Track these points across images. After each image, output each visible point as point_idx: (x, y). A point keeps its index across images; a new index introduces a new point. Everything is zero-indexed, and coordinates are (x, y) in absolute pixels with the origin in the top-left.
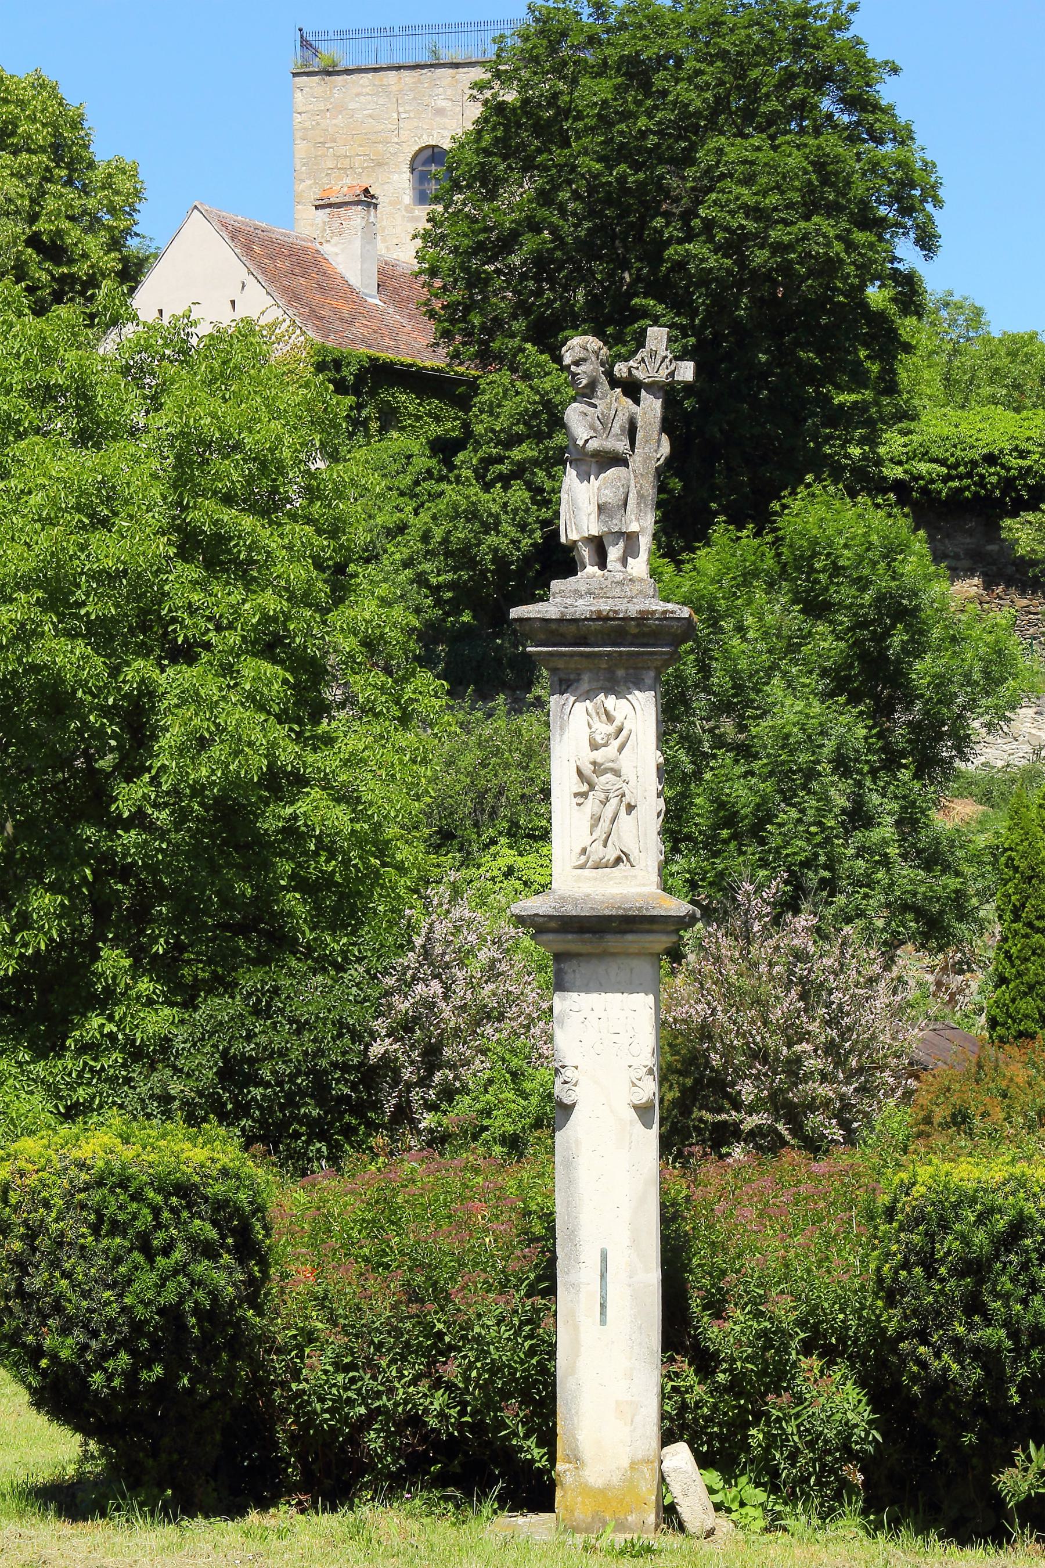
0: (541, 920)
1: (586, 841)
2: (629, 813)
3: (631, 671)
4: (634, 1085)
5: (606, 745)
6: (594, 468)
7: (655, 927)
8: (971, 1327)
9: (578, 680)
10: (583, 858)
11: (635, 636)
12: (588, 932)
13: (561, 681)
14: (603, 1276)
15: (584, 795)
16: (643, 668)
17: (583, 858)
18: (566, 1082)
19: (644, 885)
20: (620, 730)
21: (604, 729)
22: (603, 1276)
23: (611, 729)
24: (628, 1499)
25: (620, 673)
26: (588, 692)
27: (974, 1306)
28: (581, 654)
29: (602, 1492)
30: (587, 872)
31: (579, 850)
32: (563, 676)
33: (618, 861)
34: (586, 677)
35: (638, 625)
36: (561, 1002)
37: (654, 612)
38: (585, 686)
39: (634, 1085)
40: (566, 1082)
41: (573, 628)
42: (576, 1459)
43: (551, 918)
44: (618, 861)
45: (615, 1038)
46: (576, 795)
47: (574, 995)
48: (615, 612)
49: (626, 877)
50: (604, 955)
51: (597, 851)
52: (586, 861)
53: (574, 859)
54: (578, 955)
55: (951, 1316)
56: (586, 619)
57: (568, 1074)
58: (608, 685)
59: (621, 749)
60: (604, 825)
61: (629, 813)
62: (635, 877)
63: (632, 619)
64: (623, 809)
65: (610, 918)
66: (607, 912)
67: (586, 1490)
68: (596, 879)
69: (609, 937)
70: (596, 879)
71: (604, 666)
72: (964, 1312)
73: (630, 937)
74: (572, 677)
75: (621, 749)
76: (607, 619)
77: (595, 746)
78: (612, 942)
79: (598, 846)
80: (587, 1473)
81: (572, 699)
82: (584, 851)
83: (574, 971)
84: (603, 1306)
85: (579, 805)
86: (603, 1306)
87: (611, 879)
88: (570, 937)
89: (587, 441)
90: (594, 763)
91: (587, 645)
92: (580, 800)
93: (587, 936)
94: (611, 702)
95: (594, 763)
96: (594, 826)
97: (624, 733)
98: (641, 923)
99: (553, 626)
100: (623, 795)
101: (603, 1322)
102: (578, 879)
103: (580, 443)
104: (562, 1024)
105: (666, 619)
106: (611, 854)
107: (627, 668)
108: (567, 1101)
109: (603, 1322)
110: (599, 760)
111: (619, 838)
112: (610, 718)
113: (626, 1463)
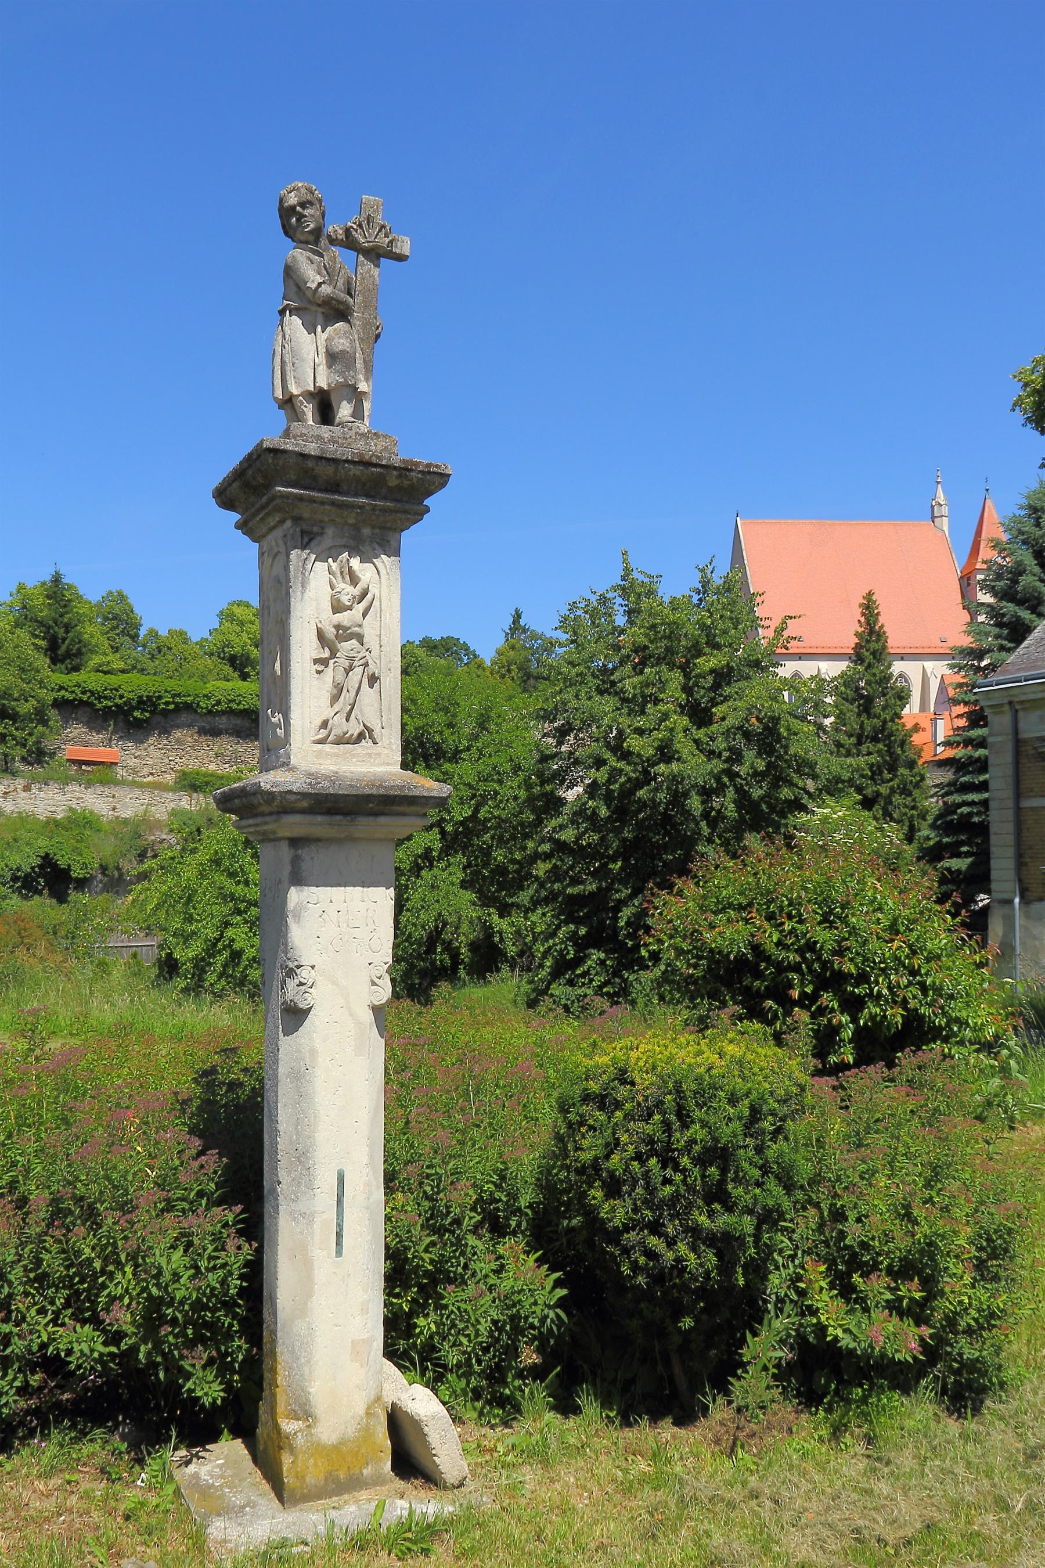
0: (292, 798)
1: (328, 713)
2: (371, 686)
3: (377, 531)
4: (374, 984)
5: (350, 608)
6: (320, 318)
7: (413, 809)
8: (711, 1214)
9: (322, 534)
10: (323, 733)
11: (391, 490)
12: (336, 813)
13: (303, 532)
14: (340, 1202)
15: (324, 662)
16: (390, 529)
17: (323, 733)
18: (301, 984)
19: (388, 764)
20: (364, 593)
21: (347, 592)
22: (340, 1202)
23: (357, 591)
24: (363, 1451)
25: (366, 531)
26: (330, 548)
27: (717, 1196)
28: (333, 503)
29: (336, 1447)
30: (327, 748)
31: (318, 722)
32: (305, 527)
33: (361, 737)
34: (330, 531)
35: (400, 476)
36: (295, 896)
37: (418, 464)
38: (329, 538)
39: (374, 984)
40: (301, 984)
41: (330, 470)
42: (305, 1413)
43: (304, 795)
44: (361, 737)
45: (356, 932)
46: (316, 661)
47: (313, 889)
48: (378, 457)
49: (370, 755)
50: (352, 839)
51: (339, 725)
52: (327, 735)
53: (313, 733)
54: (318, 840)
55: (690, 1205)
56: (347, 461)
57: (304, 974)
58: (352, 543)
59: (364, 615)
60: (346, 697)
61: (371, 686)
62: (379, 754)
63: (395, 468)
64: (365, 680)
65: (368, 798)
66: (367, 791)
67: (319, 1449)
68: (337, 755)
69: (362, 821)
70: (337, 755)
71: (351, 521)
72: (704, 1199)
73: (383, 820)
74: (315, 529)
75: (364, 615)
76: (368, 464)
77: (338, 608)
78: (364, 826)
79: (340, 719)
80: (320, 1430)
81: (313, 557)
82: (325, 724)
83: (312, 858)
84: (339, 1235)
85: (318, 672)
86: (339, 1235)
87: (353, 756)
88: (319, 818)
89: (320, 285)
90: (338, 627)
91: (340, 493)
92: (321, 668)
93: (338, 818)
94: (355, 563)
95: (338, 627)
96: (335, 699)
97: (369, 596)
98: (400, 804)
99: (310, 464)
100: (366, 665)
101: (339, 1253)
102: (319, 755)
103: (314, 286)
104: (298, 917)
105: (429, 472)
106: (355, 729)
107: (373, 527)
108: (303, 1005)
109: (339, 1253)
110: (346, 623)
111: (361, 711)
112: (354, 580)
113: (361, 1410)
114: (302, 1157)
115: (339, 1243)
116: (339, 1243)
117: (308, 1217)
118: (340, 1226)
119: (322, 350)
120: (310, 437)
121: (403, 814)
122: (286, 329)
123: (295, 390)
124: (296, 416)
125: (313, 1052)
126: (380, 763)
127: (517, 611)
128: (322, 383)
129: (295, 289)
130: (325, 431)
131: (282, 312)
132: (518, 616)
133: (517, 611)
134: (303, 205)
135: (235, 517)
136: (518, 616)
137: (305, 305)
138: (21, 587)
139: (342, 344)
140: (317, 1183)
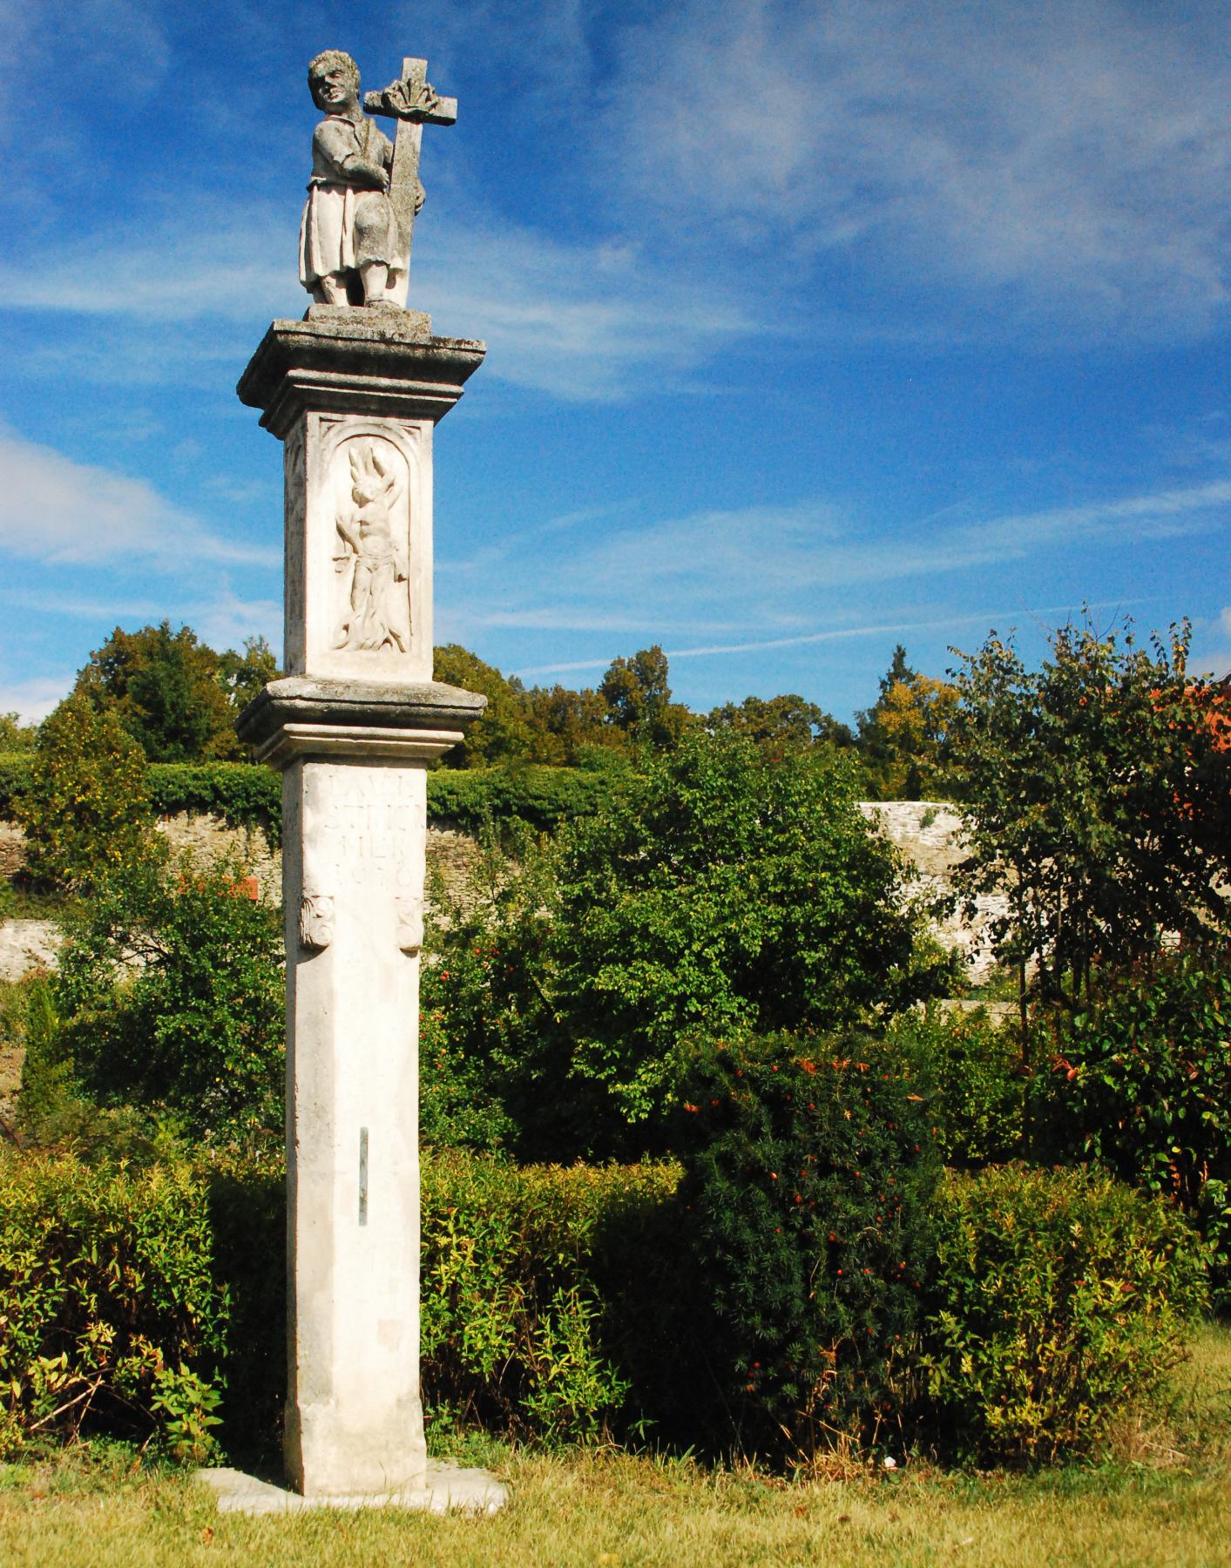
14: (363, 1163)
21: (370, 484)
22: (363, 1163)
84: (363, 1201)
86: (363, 1201)
97: (395, 488)
101: (363, 1220)
109: (363, 1220)
114: (321, 1111)
115: (363, 1210)
116: (363, 1210)
117: (328, 1176)
118: (363, 1190)
119: (350, 227)
120: (336, 315)
121: (396, 692)
122: (314, 207)
123: (320, 270)
124: (322, 295)
125: (331, 994)
126: (410, 674)
127: (899, 649)
128: (350, 262)
129: (322, 163)
130: (362, 311)
131: (310, 189)
132: (900, 655)
133: (899, 649)
134: (332, 75)
135: (258, 413)
136: (900, 655)
137: (333, 179)
138: (118, 634)
139: (372, 219)
140: (337, 1140)
